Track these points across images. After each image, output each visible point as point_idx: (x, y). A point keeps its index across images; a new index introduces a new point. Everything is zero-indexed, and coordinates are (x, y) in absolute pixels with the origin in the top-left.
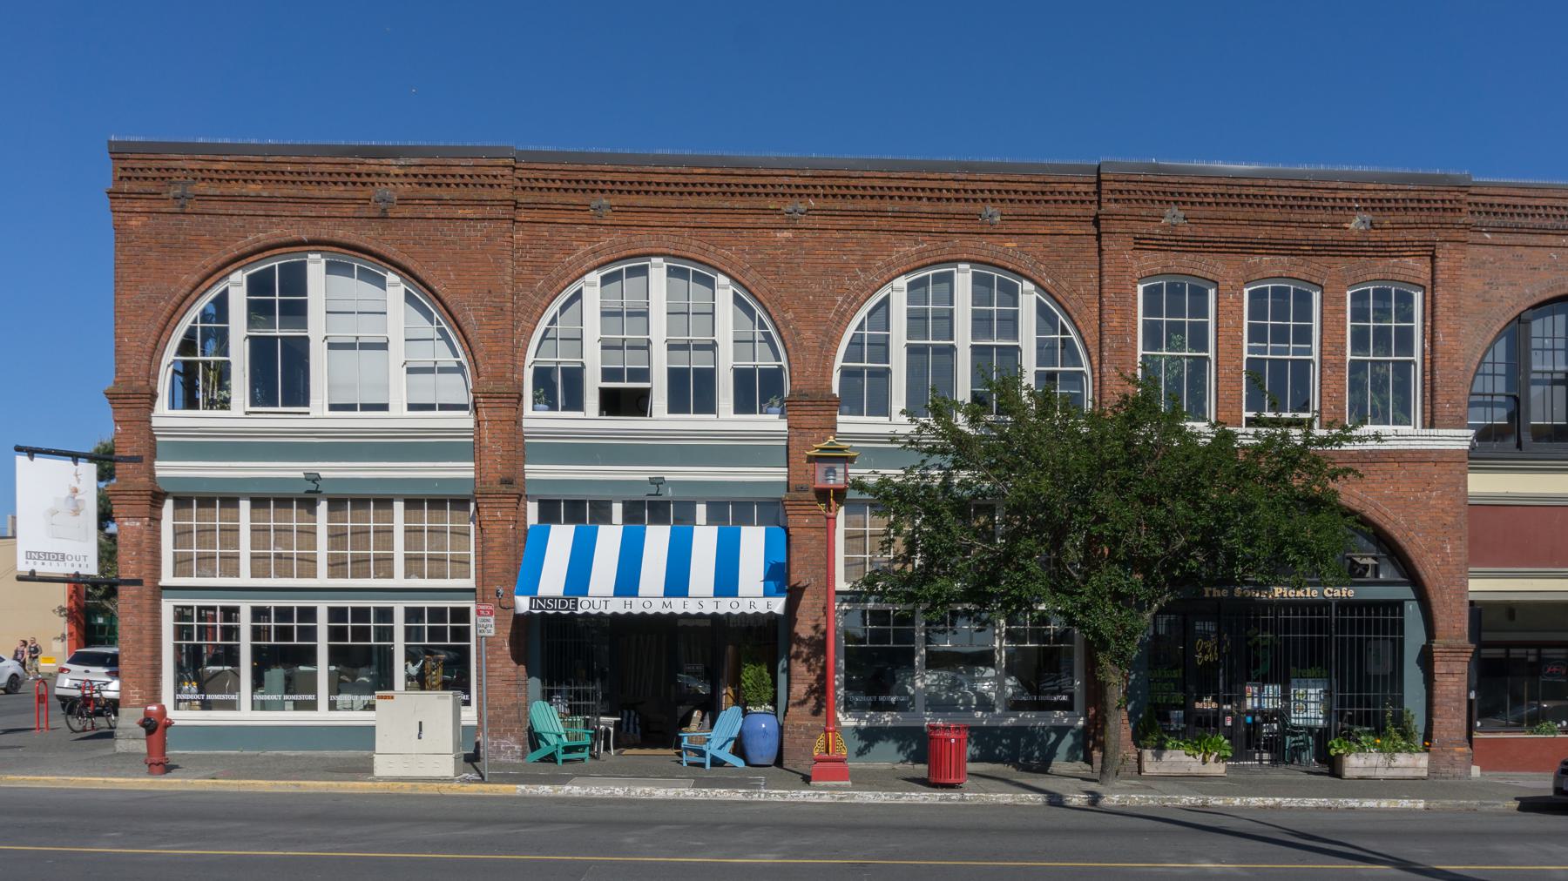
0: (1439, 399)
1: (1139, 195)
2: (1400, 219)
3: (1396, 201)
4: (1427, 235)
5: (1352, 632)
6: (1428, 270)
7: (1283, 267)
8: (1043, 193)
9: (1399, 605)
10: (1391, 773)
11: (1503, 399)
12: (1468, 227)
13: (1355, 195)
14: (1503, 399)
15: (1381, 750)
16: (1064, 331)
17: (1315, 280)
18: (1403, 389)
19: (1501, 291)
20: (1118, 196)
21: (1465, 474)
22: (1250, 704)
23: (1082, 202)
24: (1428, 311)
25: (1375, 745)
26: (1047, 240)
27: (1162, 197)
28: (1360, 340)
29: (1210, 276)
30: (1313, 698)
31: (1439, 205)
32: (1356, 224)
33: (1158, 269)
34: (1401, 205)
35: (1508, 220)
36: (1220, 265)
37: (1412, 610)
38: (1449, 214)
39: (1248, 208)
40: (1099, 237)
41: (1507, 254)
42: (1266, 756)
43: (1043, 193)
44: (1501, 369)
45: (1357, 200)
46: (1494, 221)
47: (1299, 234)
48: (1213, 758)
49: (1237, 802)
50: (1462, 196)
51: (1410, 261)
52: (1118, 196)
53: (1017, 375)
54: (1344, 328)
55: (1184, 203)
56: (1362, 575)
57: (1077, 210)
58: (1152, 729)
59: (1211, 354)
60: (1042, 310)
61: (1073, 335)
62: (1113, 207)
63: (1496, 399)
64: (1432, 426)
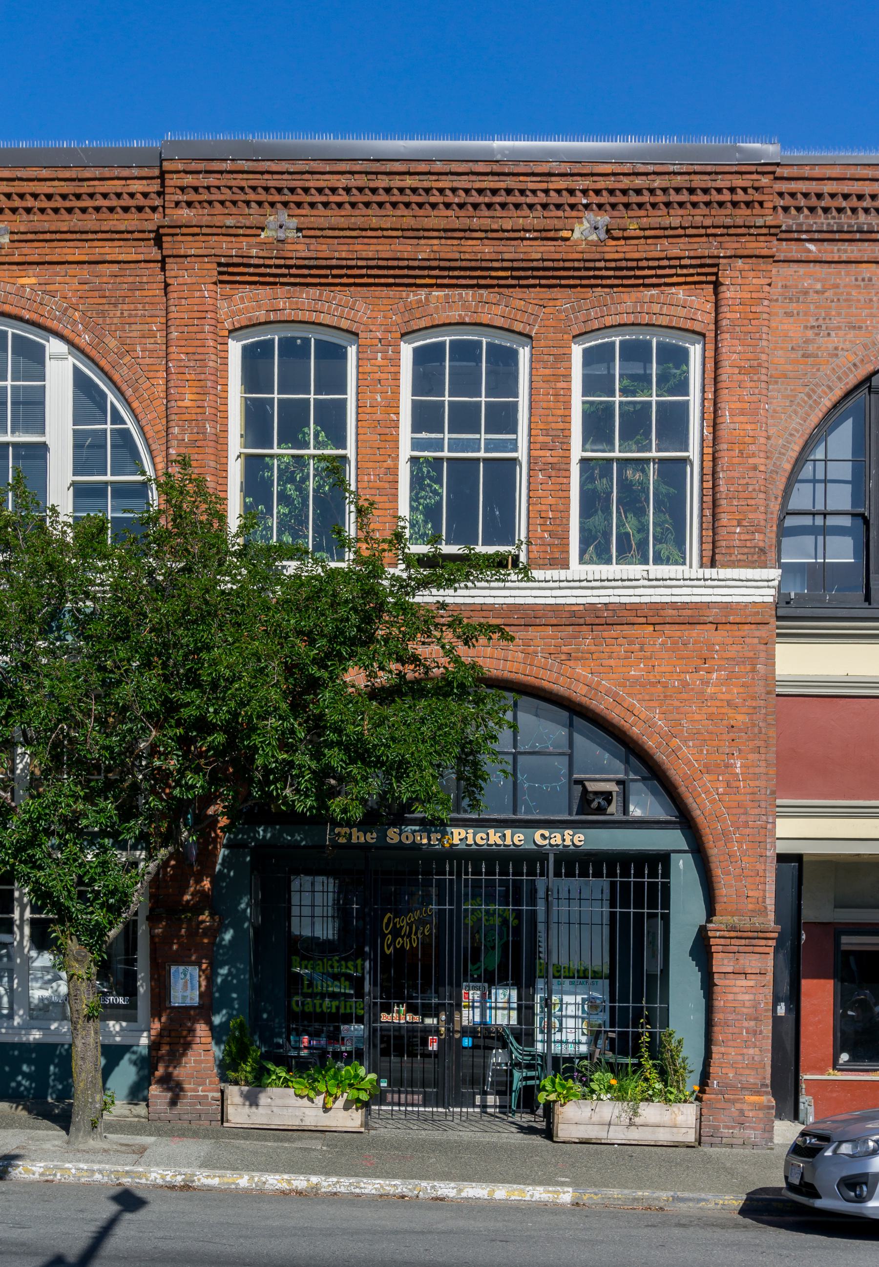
0: (724, 519)
1: (227, 195)
2: (654, 222)
3: (652, 191)
4: (705, 248)
5: (639, 904)
6: (710, 307)
7: (465, 308)
8: (78, 197)
9: (660, 861)
10: (635, 1135)
11: (846, 521)
12: (774, 232)
13: (582, 183)
14: (846, 521)
15: (620, 1095)
16: (117, 418)
17: (518, 327)
18: (673, 507)
19: (835, 339)
20: (192, 196)
21: (768, 645)
22: (469, 1017)
23: (140, 209)
24: (710, 374)
25: (610, 1088)
26: (84, 272)
27: (263, 196)
28: (597, 425)
29: (344, 324)
30: (571, 1010)
31: (726, 196)
32: (584, 231)
33: (261, 315)
34: (660, 198)
35: (846, 220)
36: (360, 305)
37: (683, 867)
38: (744, 211)
39: (401, 211)
40: (163, 262)
41: (844, 276)
42: (491, 1099)
43: (78, 197)
44: (845, 471)
45: (585, 192)
46: (821, 221)
47: (487, 250)
48: (340, 1103)
49: (243, 1181)
50: (765, 181)
51: (680, 293)
52: (192, 196)
53: (222, 518)
54: (568, 406)
55: (299, 205)
56: (601, 810)
57: (131, 221)
58: (255, 1057)
59: (350, 451)
60: (81, 382)
61: (130, 424)
62: (185, 214)
63: (832, 521)
64: (713, 564)
